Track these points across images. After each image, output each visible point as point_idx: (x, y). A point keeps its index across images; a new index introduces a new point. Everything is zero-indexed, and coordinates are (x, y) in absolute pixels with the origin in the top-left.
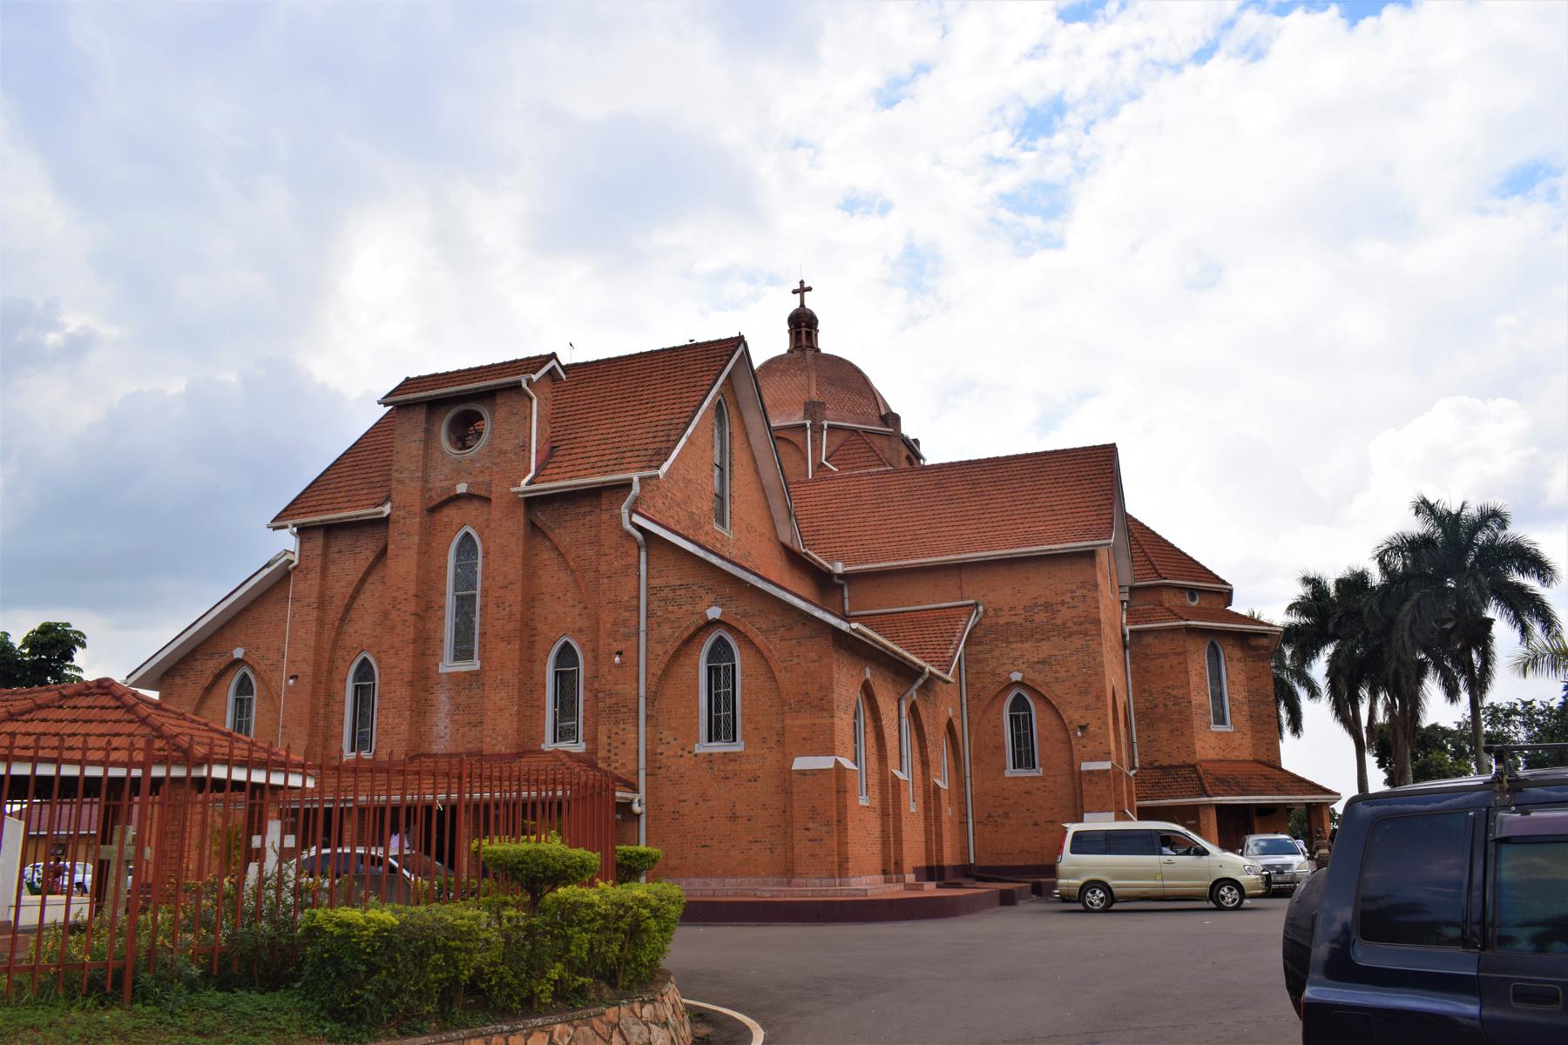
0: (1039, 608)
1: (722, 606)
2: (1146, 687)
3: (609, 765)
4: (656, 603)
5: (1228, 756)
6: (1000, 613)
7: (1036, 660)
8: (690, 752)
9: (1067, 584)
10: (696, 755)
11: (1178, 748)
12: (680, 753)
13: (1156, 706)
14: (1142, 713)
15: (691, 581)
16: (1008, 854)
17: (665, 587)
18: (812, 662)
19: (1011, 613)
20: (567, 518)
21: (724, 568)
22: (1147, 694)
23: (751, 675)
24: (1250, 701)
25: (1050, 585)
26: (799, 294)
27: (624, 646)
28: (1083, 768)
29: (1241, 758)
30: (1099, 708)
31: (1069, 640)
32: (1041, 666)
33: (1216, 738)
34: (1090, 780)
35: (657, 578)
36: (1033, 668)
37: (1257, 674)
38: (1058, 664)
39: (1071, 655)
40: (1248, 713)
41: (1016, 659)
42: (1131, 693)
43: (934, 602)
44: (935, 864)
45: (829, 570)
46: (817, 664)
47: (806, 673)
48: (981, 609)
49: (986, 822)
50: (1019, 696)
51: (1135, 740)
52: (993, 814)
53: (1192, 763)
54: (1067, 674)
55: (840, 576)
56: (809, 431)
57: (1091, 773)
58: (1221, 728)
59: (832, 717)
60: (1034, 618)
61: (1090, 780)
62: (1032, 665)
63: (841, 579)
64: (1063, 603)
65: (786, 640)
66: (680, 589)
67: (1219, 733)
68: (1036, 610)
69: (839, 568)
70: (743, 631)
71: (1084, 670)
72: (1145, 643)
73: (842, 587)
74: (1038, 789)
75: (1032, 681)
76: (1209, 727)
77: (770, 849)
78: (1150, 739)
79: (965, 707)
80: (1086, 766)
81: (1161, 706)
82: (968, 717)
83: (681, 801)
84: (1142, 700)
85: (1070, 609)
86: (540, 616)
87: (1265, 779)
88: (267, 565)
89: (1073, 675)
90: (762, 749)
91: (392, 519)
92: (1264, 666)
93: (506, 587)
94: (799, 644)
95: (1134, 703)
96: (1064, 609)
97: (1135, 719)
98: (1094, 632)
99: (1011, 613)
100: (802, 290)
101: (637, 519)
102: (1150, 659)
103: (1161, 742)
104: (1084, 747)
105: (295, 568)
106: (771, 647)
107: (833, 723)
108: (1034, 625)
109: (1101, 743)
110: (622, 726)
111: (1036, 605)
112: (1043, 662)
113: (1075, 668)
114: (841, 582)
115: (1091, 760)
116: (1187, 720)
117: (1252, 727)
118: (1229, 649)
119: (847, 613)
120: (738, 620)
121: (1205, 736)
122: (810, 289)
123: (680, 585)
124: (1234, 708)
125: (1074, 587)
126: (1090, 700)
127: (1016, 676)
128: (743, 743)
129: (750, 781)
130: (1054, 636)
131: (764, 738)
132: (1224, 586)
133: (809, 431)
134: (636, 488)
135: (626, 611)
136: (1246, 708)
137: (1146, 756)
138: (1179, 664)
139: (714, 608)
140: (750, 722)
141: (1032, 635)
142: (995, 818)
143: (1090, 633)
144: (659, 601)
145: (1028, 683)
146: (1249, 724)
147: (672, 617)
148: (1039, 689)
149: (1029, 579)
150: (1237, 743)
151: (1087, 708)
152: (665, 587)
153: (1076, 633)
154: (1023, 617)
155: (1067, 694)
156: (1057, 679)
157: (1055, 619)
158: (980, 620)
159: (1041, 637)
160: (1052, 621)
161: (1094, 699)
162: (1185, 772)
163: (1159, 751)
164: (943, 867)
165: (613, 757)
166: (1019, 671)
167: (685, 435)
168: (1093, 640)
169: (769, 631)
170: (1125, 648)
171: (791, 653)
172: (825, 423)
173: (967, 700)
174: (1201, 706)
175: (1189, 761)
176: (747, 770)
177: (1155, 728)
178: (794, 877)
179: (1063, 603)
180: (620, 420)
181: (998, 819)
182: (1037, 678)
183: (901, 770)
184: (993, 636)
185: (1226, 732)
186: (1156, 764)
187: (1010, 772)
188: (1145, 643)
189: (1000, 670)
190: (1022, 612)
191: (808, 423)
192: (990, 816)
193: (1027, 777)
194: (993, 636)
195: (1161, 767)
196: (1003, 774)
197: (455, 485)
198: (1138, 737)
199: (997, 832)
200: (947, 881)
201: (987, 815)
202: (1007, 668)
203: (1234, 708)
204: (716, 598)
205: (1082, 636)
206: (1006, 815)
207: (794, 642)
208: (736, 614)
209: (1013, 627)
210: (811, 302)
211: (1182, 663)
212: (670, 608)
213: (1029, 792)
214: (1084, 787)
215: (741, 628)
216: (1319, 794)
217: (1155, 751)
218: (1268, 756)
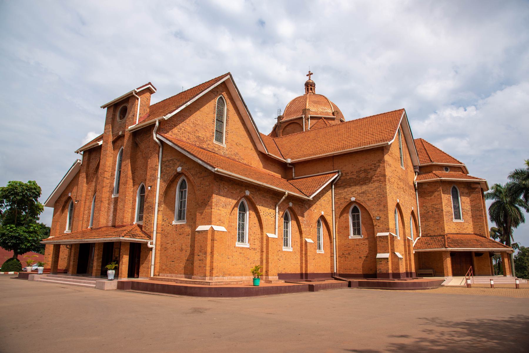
0: (362, 171)
1: (182, 166)
2: (424, 204)
3: (145, 229)
4: (164, 167)
5: (461, 232)
6: (347, 175)
7: (361, 192)
8: (171, 224)
9: (373, 161)
10: (172, 226)
11: (438, 228)
12: (168, 225)
13: (428, 212)
14: (423, 215)
15: (174, 157)
16: (350, 269)
17: (167, 161)
18: (207, 186)
19: (352, 174)
20: (144, 139)
21: (179, 151)
22: (425, 207)
23: (190, 193)
24: (472, 210)
25: (366, 162)
26: (308, 76)
27: (152, 184)
28: (377, 235)
29: (468, 233)
30: (385, 211)
31: (373, 184)
32: (362, 194)
33: (456, 225)
34: (380, 240)
35: (165, 157)
36: (359, 195)
37: (475, 199)
38: (369, 193)
39: (374, 190)
40: (471, 215)
41: (353, 192)
42: (418, 207)
43: (324, 172)
44: (304, 272)
45: (285, 162)
46: (208, 187)
47: (205, 191)
48: (340, 173)
49: (342, 256)
50: (355, 207)
51: (420, 226)
52: (344, 253)
53: (443, 234)
54: (372, 197)
55: (290, 164)
56: (304, 119)
57: (380, 237)
58: (458, 221)
59: (212, 209)
60: (360, 176)
61: (380, 240)
62: (359, 194)
63: (291, 165)
64: (371, 169)
65: (200, 178)
66: (171, 161)
67: (457, 223)
68: (361, 173)
69: (289, 161)
70: (187, 175)
71: (379, 196)
72: (424, 187)
73: (292, 168)
74: (362, 244)
75: (359, 200)
76: (452, 220)
77: (192, 263)
78: (426, 225)
79: (334, 212)
80: (379, 234)
81: (430, 212)
82: (335, 215)
83: (167, 243)
84: (423, 210)
85: (374, 171)
86: (136, 175)
87: (477, 241)
88: (73, 165)
89: (375, 198)
90: (192, 223)
91: (103, 145)
92: (477, 196)
93: (126, 166)
94: (204, 179)
95: (420, 211)
96: (371, 171)
97: (420, 217)
98: (383, 180)
99: (352, 174)
100: (310, 74)
101: (158, 136)
102: (426, 194)
103: (431, 226)
104: (379, 226)
105: (81, 165)
106: (195, 181)
107: (212, 211)
108: (360, 178)
109: (385, 225)
110: (149, 214)
111: (361, 170)
112: (363, 193)
113: (376, 195)
114: (290, 166)
115: (381, 232)
116: (441, 217)
117: (472, 220)
118: (462, 189)
119: (293, 178)
120: (186, 171)
121: (451, 224)
122: (312, 74)
123: (171, 160)
124: (464, 213)
125: (375, 163)
126: (382, 207)
127: (353, 199)
128: (186, 220)
129: (187, 235)
130: (368, 182)
131: (192, 218)
132: (461, 165)
133: (304, 119)
134: (157, 123)
135: (154, 171)
136: (470, 212)
137: (425, 232)
138: (438, 195)
139: (180, 167)
140: (189, 212)
141: (359, 183)
142: (345, 255)
143: (381, 180)
144: (165, 166)
145: (357, 201)
146: (471, 219)
147: (168, 172)
148: (361, 204)
149: (358, 160)
150: (465, 227)
151: (380, 211)
152: (167, 161)
153: (376, 181)
154: (356, 175)
155: (372, 205)
156: (369, 199)
157: (368, 175)
158: (340, 177)
159: (363, 183)
160: (367, 177)
161: (383, 207)
162: (439, 238)
163: (430, 230)
164: (307, 273)
165: (147, 226)
166: (354, 197)
167: (185, 105)
168: (383, 183)
169: (194, 175)
170: (416, 190)
171: (201, 183)
172: (309, 116)
173: (335, 208)
174: (448, 212)
175: (442, 234)
176: (187, 231)
177: (428, 221)
178: (193, 275)
179: (371, 169)
180: (327, 141)
181: (346, 255)
182: (361, 199)
183: (275, 234)
184: (345, 184)
185: (460, 222)
186: (429, 235)
187: (352, 236)
188: (424, 187)
189: (347, 197)
190: (356, 173)
191: (303, 116)
192: (343, 254)
193: (357, 239)
194: (345, 184)
195: (430, 236)
196: (348, 238)
197: (119, 132)
198: (421, 224)
199: (346, 260)
200: (413, 278)
201: (342, 254)
202: (350, 196)
203: (464, 213)
204: (180, 164)
205: (378, 182)
206: (349, 254)
207: (202, 179)
208: (185, 169)
209: (352, 180)
210: (313, 79)
211: (439, 195)
212: (168, 169)
213: (358, 245)
214: (378, 243)
215: (187, 175)
216: (503, 248)
217: (428, 230)
218: (480, 232)
